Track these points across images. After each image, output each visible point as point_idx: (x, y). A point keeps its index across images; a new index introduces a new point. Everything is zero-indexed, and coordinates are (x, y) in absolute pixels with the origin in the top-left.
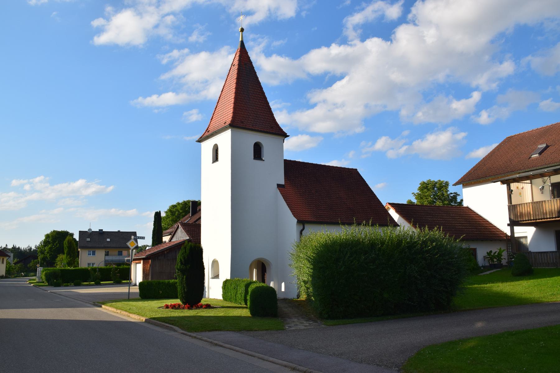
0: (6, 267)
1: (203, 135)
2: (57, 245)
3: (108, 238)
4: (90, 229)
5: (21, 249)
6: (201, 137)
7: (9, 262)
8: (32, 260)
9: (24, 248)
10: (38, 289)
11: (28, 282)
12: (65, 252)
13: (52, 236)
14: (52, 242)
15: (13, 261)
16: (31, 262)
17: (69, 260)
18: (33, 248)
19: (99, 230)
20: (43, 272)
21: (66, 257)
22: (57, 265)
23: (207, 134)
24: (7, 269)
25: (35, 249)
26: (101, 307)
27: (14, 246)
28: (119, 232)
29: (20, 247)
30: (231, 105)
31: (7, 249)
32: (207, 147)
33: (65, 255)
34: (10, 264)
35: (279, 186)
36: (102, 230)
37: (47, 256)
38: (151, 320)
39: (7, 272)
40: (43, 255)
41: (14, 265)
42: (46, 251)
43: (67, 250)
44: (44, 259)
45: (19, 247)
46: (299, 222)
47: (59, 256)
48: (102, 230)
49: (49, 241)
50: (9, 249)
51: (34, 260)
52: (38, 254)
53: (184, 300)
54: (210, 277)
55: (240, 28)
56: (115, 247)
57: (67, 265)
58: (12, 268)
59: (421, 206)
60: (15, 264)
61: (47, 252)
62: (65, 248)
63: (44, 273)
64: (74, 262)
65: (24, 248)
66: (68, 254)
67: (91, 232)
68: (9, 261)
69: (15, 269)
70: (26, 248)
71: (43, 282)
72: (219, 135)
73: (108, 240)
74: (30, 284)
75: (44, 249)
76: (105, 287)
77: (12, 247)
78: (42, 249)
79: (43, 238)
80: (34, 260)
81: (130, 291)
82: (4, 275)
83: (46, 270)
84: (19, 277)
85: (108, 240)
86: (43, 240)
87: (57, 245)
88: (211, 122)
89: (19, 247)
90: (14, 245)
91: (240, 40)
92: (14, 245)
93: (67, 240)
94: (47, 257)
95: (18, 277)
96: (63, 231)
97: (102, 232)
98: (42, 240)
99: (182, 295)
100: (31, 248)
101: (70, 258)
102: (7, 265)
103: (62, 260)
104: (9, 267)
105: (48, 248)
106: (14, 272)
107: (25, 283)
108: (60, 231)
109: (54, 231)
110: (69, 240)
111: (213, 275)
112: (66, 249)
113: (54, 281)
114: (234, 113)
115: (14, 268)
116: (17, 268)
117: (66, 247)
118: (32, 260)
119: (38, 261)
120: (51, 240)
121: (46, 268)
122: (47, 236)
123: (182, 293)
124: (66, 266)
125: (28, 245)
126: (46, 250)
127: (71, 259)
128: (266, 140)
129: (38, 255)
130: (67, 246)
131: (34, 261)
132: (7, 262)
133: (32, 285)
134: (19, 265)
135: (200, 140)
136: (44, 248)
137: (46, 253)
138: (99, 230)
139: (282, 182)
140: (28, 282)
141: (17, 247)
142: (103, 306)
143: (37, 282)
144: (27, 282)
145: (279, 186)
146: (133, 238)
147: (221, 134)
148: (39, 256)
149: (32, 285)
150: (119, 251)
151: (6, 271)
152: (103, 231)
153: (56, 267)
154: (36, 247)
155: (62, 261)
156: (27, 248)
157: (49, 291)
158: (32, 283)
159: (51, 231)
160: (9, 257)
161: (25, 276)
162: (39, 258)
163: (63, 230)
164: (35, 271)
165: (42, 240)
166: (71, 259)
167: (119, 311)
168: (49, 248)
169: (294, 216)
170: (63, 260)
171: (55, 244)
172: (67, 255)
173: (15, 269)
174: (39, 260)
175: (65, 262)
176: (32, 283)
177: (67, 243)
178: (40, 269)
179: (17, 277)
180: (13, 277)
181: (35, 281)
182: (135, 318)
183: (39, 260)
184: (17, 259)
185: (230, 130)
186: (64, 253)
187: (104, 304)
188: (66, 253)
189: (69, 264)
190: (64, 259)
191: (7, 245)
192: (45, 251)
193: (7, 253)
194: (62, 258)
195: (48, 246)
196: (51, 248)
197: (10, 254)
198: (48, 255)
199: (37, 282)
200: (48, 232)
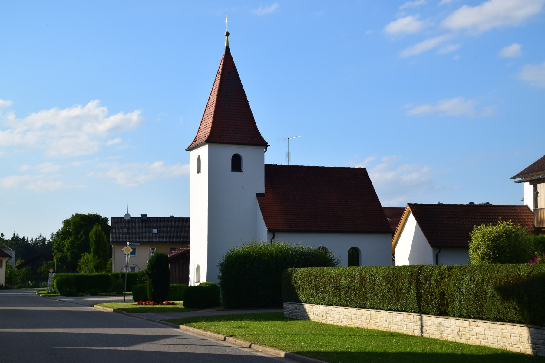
0: (6, 272)
1: (192, 144)
2: (82, 237)
3: (155, 228)
4: (128, 215)
5: (27, 241)
6: (190, 146)
7: (10, 266)
8: (44, 262)
9: (32, 239)
10: (47, 299)
11: (36, 293)
12: (92, 250)
13: (73, 223)
14: (74, 233)
15: (15, 263)
16: (43, 265)
17: (98, 261)
18: (48, 238)
19: (141, 215)
20: (55, 278)
21: (94, 257)
22: (80, 269)
23: (194, 144)
24: (8, 276)
25: (51, 240)
26: (93, 306)
27: (16, 235)
28: (172, 217)
29: (26, 238)
30: (210, 119)
31: (3, 239)
32: (194, 154)
33: (92, 254)
34: (12, 268)
35: (258, 195)
36: (146, 215)
37: (67, 255)
38: (117, 310)
39: (6, 280)
40: (61, 253)
41: (16, 269)
42: (65, 248)
43: (94, 247)
44: (62, 260)
45: (24, 237)
46: (269, 231)
47: (83, 256)
48: (146, 215)
49: (69, 232)
50: (6, 240)
51: (47, 262)
52: (53, 252)
53: (151, 299)
54: (195, 282)
55: (225, 33)
56: (164, 242)
57: (94, 270)
58: (15, 275)
59: (470, 206)
60: (19, 267)
61: (67, 249)
62: (90, 244)
63: (56, 280)
64: (105, 265)
65: (32, 239)
66: (96, 252)
67: (129, 218)
68: (10, 264)
69: (19, 275)
70: (36, 239)
71: (55, 292)
72: (196, 150)
73: (155, 231)
74: (38, 295)
75: (63, 244)
76: (113, 297)
77: (12, 238)
78: (59, 244)
79: (59, 226)
80: (47, 262)
81: (124, 297)
82: (4, 285)
83: (58, 276)
84: (25, 287)
85: (155, 231)
86: (61, 229)
87: (82, 237)
88: (199, 131)
89: (24, 237)
90: (14, 234)
91: (226, 45)
92: (14, 234)
93: (94, 232)
94: (66, 257)
95: (23, 288)
96: (91, 215)
97: (146, 219)
98: (60, 230)
99: (150, 294)
100: (44, 240)
101: (99, 259)
102: (8, 270)
103: (86, 263)
104: (10, 273)
105: (68, 243)
106: (17, 280)
107: (33, 294)
108: (87, 214)
109: (77, 215)
110: (96, 231)
111: (197, 280)
112: (92, 244)
113: (66, 290)
114: (213, 127)
115: (17, 274)
116: (21, 274)
117: (93, 243)
118: (44, 262)
119: (54, 262)
120: (73, 229)
121: (59, 274)
122: (67, 223)
123: (150, 293)
124: (93, 272)
125: (40, 234)
126: (65, 245)
127: (100, 260)
128: (246, 152)
129: (53, 254)
130: (94, 241)
131: (46, 263)
132: (6, 266)
133: (41, 295)
134: (24, 270)
135: (190, 149)
136: (63, 243)
137: (66, 251)
138: (141, 215)
139: (262, 191)
140: (36, 293)
141: (21, 237)
142: (95, 306)
143: (48, 292)
144: (36, 292)
145: (258, 195)
146: (128, 244)
147: (202, 147)
148: (55, 255)
149: (41, 295)
150: (170, 248)
151: (6, 278)
152: (148, 216)
153: (78, 272)
154: (53, 237)
155: (87, 263)
156: (38, 240)
157: (58, 300)
158: (41, 294)
159: (73, 216)
160: (10, 257)
161: (34, 286)
162: (54, 258)
163: (91, 213)
164: (46, 279)
165: (60, 230)
166: (100, 260)
167: (102, 308)
168: (70, 243)
169: (266, 225)
170: (88, 261)
171: (79, 236)
172: (94, 254)
173: (19, 275)
174: (55, 261)
175: (91, 264)
176: (41, 294)
177: (93, 236)
178: (52, 275)
179: (21, 287)
180: (16, 288)
181: (46, 292)
182: (109, 310)
183: (55, 261)
184: (21, 260)
185: (207, 145)
186: (90, 252)
187: (95, 304)
188: (93, 252)
189: (98, 268)
190: (90, 260)
191: (2, 234)
192: (64, 247)
193: (6, 252)
194: (87, 259)
195: (69, 239)
196: (72, 243)
197: (11, 252)
198: (69, 253)
199: (48, 293)
200: (69, 217)
